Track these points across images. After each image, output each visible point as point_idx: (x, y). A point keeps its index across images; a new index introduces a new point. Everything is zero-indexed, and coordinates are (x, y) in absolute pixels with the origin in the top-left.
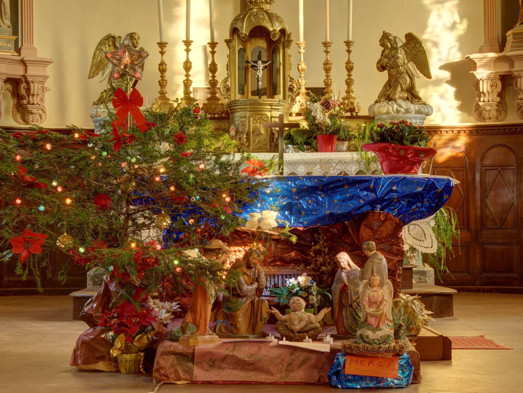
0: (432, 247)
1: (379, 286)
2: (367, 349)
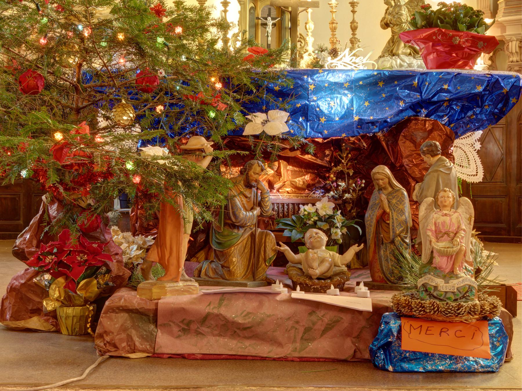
0: (476, 175)
1: (452, 207)
2: (438, 309)
